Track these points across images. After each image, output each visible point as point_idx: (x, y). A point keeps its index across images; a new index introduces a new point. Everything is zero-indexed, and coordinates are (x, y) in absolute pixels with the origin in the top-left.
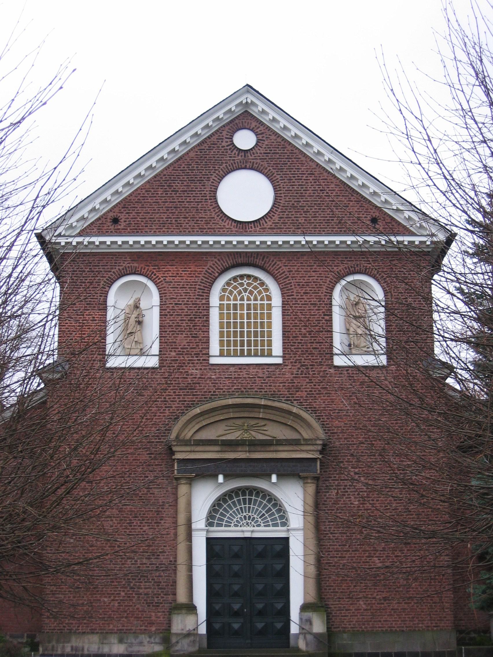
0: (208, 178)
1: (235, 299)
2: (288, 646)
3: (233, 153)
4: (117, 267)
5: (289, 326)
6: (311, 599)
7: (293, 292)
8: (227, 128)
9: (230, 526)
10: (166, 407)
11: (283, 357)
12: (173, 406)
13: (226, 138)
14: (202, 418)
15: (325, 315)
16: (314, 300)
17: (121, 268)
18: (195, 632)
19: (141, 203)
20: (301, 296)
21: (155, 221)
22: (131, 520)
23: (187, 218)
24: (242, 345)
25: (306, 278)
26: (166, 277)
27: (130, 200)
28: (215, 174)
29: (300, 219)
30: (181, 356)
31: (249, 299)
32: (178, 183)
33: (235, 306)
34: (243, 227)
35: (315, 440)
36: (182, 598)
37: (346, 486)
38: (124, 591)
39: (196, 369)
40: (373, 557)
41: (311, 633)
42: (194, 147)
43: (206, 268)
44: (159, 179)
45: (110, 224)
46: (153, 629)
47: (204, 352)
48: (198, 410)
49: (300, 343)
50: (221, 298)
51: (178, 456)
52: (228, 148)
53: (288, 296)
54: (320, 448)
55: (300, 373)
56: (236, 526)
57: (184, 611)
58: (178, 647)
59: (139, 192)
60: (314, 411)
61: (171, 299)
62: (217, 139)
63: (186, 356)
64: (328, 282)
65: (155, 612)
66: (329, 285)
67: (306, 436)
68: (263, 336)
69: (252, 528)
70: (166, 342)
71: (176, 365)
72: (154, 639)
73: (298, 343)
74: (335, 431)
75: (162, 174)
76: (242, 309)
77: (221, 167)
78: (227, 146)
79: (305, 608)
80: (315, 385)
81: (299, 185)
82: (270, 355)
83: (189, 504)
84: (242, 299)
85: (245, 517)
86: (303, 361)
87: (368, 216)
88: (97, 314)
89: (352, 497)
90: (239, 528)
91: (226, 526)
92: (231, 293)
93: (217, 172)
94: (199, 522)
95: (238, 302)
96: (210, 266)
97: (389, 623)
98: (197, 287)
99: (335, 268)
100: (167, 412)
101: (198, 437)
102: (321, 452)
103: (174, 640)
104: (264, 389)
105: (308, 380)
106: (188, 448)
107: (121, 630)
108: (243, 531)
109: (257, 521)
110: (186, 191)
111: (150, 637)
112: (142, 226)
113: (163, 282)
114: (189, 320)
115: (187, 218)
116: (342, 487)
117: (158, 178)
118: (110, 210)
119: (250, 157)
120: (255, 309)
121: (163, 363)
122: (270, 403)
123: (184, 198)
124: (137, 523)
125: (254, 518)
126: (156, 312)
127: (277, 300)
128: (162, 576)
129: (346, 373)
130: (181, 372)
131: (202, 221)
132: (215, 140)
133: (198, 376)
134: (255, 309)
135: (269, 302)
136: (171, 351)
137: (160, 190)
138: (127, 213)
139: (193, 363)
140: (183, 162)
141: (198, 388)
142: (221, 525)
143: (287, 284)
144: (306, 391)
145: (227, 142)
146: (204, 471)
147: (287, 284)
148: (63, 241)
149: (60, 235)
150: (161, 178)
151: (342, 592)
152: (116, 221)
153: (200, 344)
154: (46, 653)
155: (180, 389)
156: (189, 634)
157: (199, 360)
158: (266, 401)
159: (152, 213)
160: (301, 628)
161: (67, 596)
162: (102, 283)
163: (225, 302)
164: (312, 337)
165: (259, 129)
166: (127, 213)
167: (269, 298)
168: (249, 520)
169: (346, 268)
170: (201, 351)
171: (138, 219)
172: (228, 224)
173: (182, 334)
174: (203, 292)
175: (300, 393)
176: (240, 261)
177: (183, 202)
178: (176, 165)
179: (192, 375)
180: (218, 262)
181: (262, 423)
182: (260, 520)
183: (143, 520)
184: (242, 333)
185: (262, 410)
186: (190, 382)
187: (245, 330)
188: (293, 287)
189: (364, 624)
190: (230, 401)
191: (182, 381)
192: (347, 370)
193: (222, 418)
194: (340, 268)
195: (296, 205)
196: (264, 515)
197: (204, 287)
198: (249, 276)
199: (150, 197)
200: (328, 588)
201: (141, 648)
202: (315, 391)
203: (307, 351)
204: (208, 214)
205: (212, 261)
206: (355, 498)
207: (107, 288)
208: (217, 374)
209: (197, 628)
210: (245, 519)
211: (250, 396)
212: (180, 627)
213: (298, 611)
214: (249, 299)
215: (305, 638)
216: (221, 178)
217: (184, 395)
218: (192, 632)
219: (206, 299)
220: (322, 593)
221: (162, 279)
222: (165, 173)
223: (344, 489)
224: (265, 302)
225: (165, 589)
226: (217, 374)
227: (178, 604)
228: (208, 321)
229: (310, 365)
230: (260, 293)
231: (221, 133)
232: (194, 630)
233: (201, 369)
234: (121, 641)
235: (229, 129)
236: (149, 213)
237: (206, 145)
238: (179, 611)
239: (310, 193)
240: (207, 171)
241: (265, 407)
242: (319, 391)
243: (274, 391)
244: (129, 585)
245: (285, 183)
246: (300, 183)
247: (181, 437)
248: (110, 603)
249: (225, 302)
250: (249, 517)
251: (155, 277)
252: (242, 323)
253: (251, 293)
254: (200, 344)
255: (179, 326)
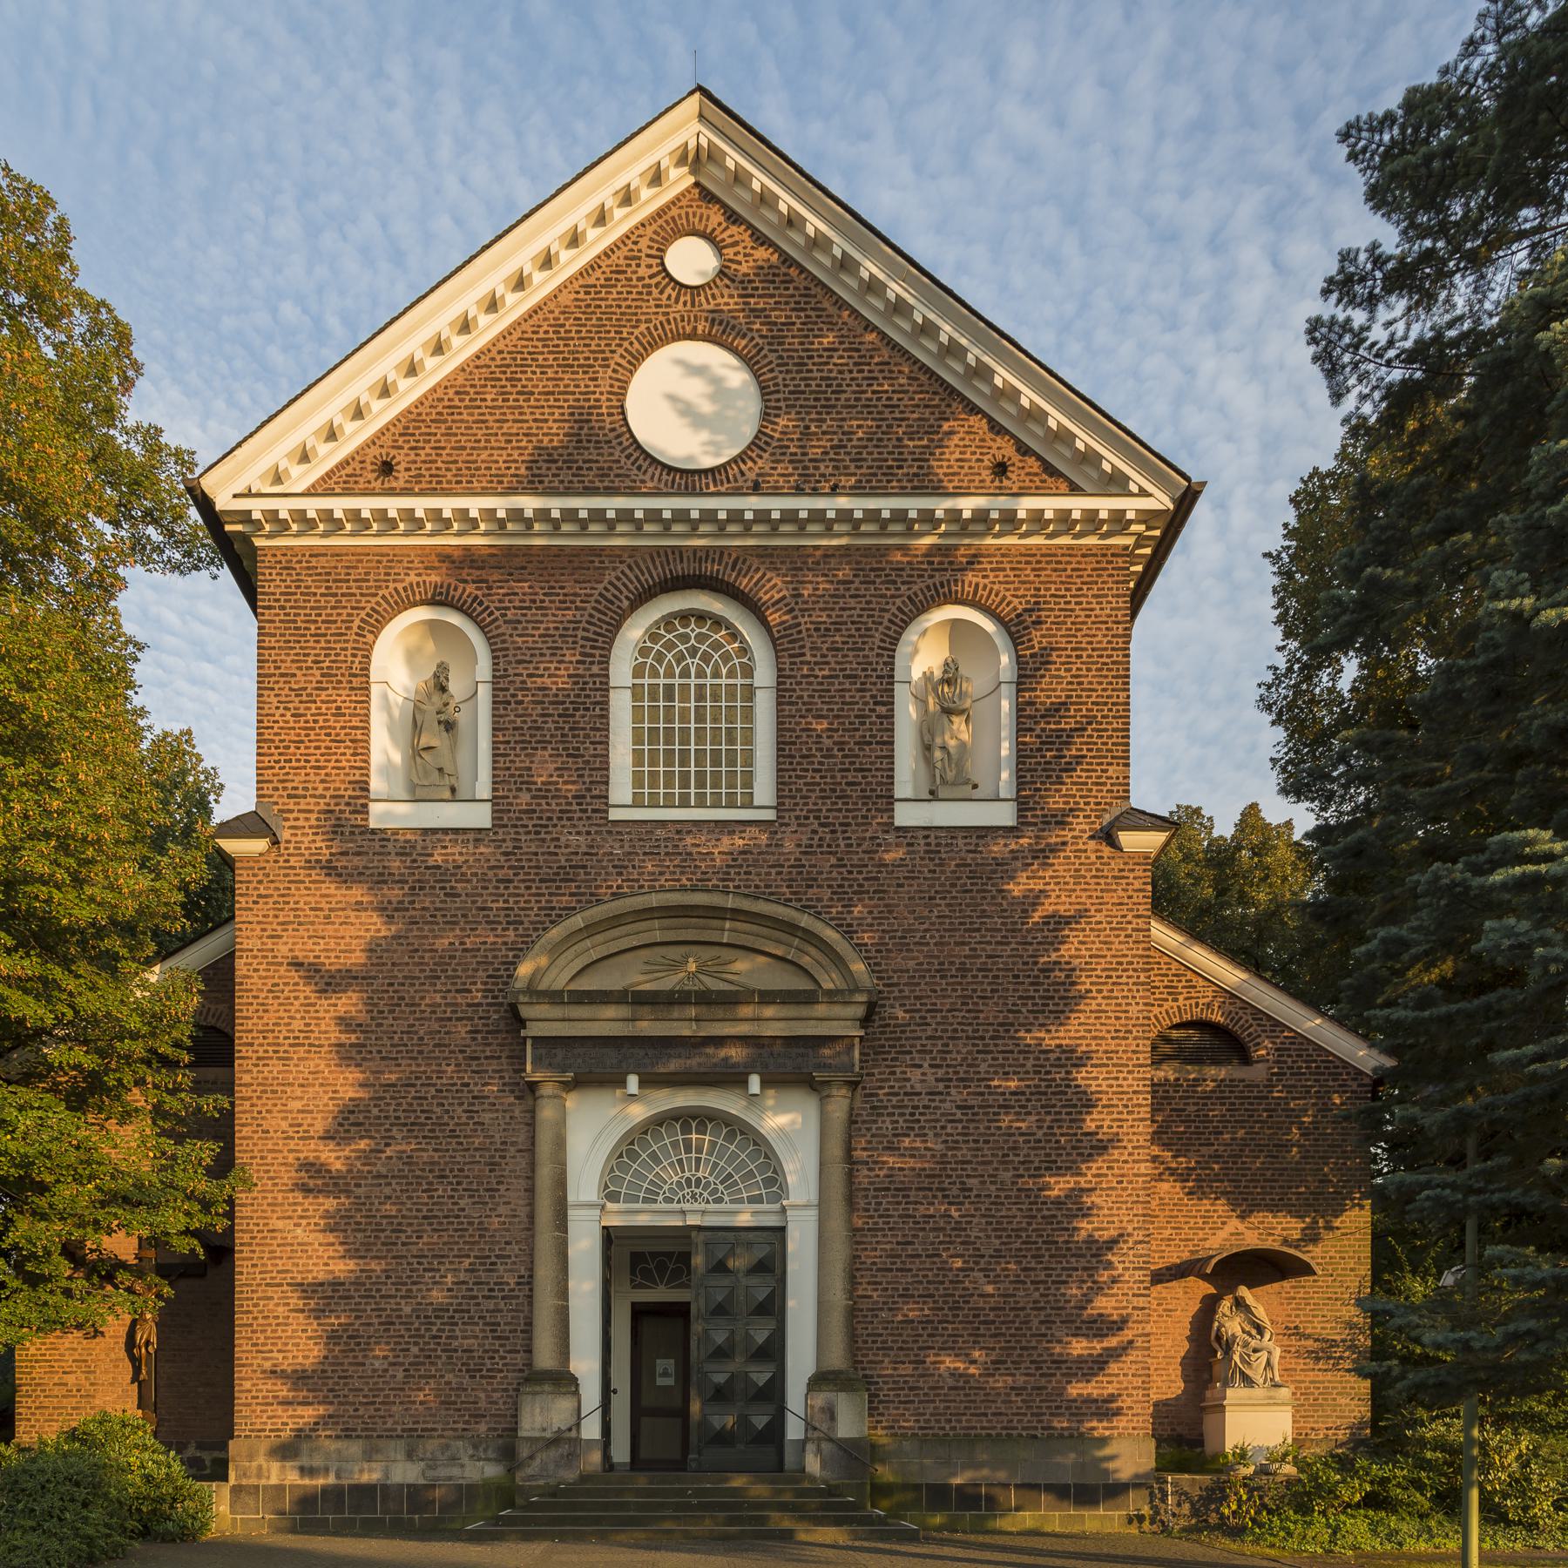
0: (604, 359)
1: (670, 673)
2: (780, 1467)
3: (665, 296)
4: (391, 585)
5: (794, 730)
6: (837, 1359)
7: (803, 647)
8: (649, 230)
9: (655, 1201)
10: (508, 923)
11: (779, 808)
12: (526, 920)
13: (648, 256)
14: (588, 943)
15: (876, 703)
16: (852, 666)
17: (400, 586)
18: (573, 1434)
19: (445, 421)
20: (823, 656)
21: (478, 469)
22: (430, 1183)
23: (556, 461)
24: (685, 784)
25: (833, 614)
26: (508, 608)
27: (419, 414)
28: (621, 351)
29: (822, 466)
30: (543, 802)
31: (701, 674)
32: (534, 373)
33: (669, 689)
34: (688, 479)
35: (852, 992)
36: (545, 1358)
37: (917, 1107)
38: (416, 1344)
39: (578, 833)
40: (972, 1270)
41: (831, 1440)
42: (570, 280)
43: (600, 586)
44: (488, 362)
45: (372, 476)
46: (483, 1428)
47: (595, 793)
48: (578, 921)
49: (819, 771)
50: (638, 672)
51: (534, 1030)
52: (653, 281)
53: (791, 656)
54: (860, 1011)
55: (815, 842)
56: (668, 1200)
57: (547, 1388)
58: (533, 1468)
59: (440, 394)
60: (848, 932)
61: (519, 662)
62: (626, 258)
63: (553, 802)
64: (886, 623)
65: (485, 1390)
66: (889, 629)
67: (828, 985)
68: (732, 762)
69: (703, 1206)
70: (508, 769)
71: (530, 823)
72: (485, 1450)
73: (814, 770)
74: (895, 980)
75: (494, 350)
76: (685, 698)
77: (636, 332)
78: (650, 277)
79: (820, 1380)
80: (850, 872)
81: (822, 379)
82: (749, 805)
83: (560, 1144)
84: (685, 673)
85: (688, 1180)
86: (824, 813)
87: (985, 458)
88: (343, 697)
89: (931, 1133)
90: (675, 1206)
91: (645, 1200)
92: (660, 658)
93: (626, 344)
94: (584, 1183)
95: (677, 681)
96: (610, 583)
97: (1005, 1418)
98: (580, 633)
99: (903, 588)
100: (511, 933)
101: (585, 984)
102: (866, 1021)
103: (524, 1452)
104: (733, 880)
105: (833, 861)
106: (557, 1012)
107: (411, 1430)
108: (683, 1212)
109: (716, 1191)
110: (553, 393)
111: (475, 1447)
112: (449, 482)
113: (500, 622)
114: (560, 716)
115: (556, 461)
116: (907, 1111)
117: (484, 360)
118: (372, 442)
119: (705, 306)
120: (716, 697)
121: (501, 819)
122: (746, 905)
123: (547, 410)
124: (445, 1190)
125: (708, 1184)
126: (484, 693)
127: (764, 675)
128: (500, 1311)
129: (922, 842)
130: (543, 840)
131: (590, 469)
132: (622, 262)
133: (584, 849)
134: (716, 697)
135: (748, 681)
136: (520, 790)
137: (489, 389)
138: (412, 448)
139: (569, 819)
140: (545, 319)
141: (583, 877)
142: (635, 1199)
143: (794, 641)
144: (830, 886)
145: (650, 266)
146: (595, 1066)
147: (794, 641)
148: (256, 507)
149: (249, 494)
150: (493, 359)
151: (901, 1349)
152: (387, 468)
153: (587, 773)
154: (244, 1482)
155: (541, 881)
156: (556, 1441)
157: (586, 811)
158: (738, 899)
159: (473, 448)
160: (809, 1426)
161: (290, 1355)
162: (357, 622)
163: (646, 681)
164: (845, 756)
165: (728, 232)
166: (412, 448)
167: (748, 671)
168: (697, 1187)
169: (928, 587)
170: (589, 790)
171: (439, 464)
172: (652, 478)
173: (545, 748)
174: (593, 647)
175: (815, 890)
176: (679, 569)
177: (546, 421)
178: (525, 327)
179: (567, 846)
180: (627, 571)
181: (726, 954)
182: (721, 1187)
183: (458, 1183)
184: (684, 754)
185: (728, 925)
186: (563, 863)
187: (693, 726)
188: (804, 634)
189: (950, 1421)
190: (655, 900)
191: (545, 861)
192: (926, 837)
193: (635, 943)
194: (915, 588)
195: (813, 429)
196: (730, 1176)
197: (595, 633)
198: (701, 617)
199: (466, 407)
200: (870, 1339)
201: (456, 1472)
202: (851, 886)
203: (834, 791)
204: (606, 451)
205: (614, 569)
206: (936, 1135)
207: (370, 637)
208: (627, 845)
209: (578, 1425)
210: (689, 1186)
211: (704, 901)
212: (539, 1420)
213: (803, 1389)
214: (701, 674)
215: (819, 1450)
216: (636, 360)
217: (550, 894)
218: (567, 1435)
219: (600, 663)
220: (859, 1349)
221: (497, 613)
222: (501, 346)
223: (912, 1114)
224: (739, 681)
225: (508, 1338)
226: (627, 845)
227: (537, 1373)
228: (605, 716)
229: (841, 824)
230: (726, 658)
231: (635, 243)
232: (570, 1430)
233: (588, 833)
234: (410, 1455)
235: (655, 232)
236: (464, 448)
237: (598, 273)
238: (538, 1388)
239: (848, 400)
240: (603, 343)
241: (736, 914)
242: (860, 885)
243: (757, 887)
244: (427, 1330)
245: (788, 372)
246: (825, 374)
247: (542, 987)
248: (386, 1370)
249: (646, 681)
250: (698, 1181)
251: (479, 609)
252: (685, 732)
253: (706, 658)
254: (587, 773)
255: (538, 729)
